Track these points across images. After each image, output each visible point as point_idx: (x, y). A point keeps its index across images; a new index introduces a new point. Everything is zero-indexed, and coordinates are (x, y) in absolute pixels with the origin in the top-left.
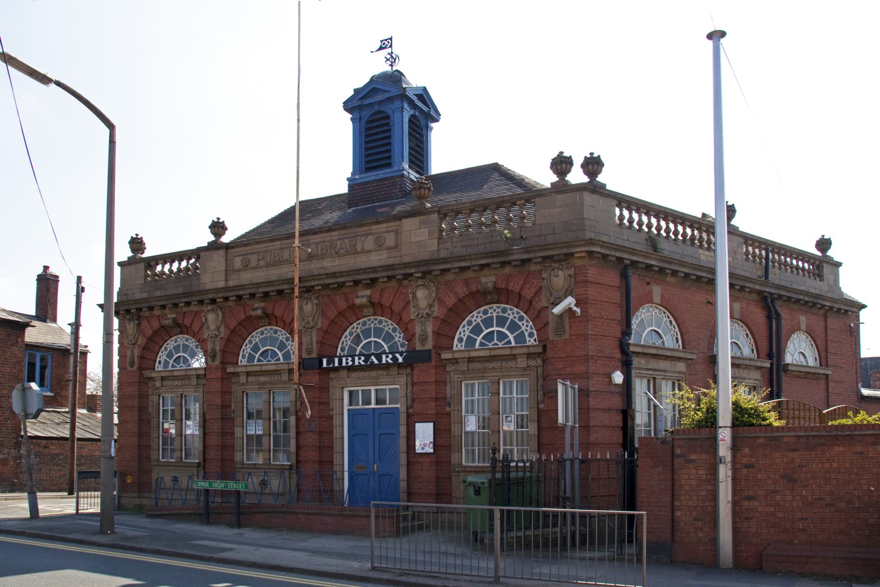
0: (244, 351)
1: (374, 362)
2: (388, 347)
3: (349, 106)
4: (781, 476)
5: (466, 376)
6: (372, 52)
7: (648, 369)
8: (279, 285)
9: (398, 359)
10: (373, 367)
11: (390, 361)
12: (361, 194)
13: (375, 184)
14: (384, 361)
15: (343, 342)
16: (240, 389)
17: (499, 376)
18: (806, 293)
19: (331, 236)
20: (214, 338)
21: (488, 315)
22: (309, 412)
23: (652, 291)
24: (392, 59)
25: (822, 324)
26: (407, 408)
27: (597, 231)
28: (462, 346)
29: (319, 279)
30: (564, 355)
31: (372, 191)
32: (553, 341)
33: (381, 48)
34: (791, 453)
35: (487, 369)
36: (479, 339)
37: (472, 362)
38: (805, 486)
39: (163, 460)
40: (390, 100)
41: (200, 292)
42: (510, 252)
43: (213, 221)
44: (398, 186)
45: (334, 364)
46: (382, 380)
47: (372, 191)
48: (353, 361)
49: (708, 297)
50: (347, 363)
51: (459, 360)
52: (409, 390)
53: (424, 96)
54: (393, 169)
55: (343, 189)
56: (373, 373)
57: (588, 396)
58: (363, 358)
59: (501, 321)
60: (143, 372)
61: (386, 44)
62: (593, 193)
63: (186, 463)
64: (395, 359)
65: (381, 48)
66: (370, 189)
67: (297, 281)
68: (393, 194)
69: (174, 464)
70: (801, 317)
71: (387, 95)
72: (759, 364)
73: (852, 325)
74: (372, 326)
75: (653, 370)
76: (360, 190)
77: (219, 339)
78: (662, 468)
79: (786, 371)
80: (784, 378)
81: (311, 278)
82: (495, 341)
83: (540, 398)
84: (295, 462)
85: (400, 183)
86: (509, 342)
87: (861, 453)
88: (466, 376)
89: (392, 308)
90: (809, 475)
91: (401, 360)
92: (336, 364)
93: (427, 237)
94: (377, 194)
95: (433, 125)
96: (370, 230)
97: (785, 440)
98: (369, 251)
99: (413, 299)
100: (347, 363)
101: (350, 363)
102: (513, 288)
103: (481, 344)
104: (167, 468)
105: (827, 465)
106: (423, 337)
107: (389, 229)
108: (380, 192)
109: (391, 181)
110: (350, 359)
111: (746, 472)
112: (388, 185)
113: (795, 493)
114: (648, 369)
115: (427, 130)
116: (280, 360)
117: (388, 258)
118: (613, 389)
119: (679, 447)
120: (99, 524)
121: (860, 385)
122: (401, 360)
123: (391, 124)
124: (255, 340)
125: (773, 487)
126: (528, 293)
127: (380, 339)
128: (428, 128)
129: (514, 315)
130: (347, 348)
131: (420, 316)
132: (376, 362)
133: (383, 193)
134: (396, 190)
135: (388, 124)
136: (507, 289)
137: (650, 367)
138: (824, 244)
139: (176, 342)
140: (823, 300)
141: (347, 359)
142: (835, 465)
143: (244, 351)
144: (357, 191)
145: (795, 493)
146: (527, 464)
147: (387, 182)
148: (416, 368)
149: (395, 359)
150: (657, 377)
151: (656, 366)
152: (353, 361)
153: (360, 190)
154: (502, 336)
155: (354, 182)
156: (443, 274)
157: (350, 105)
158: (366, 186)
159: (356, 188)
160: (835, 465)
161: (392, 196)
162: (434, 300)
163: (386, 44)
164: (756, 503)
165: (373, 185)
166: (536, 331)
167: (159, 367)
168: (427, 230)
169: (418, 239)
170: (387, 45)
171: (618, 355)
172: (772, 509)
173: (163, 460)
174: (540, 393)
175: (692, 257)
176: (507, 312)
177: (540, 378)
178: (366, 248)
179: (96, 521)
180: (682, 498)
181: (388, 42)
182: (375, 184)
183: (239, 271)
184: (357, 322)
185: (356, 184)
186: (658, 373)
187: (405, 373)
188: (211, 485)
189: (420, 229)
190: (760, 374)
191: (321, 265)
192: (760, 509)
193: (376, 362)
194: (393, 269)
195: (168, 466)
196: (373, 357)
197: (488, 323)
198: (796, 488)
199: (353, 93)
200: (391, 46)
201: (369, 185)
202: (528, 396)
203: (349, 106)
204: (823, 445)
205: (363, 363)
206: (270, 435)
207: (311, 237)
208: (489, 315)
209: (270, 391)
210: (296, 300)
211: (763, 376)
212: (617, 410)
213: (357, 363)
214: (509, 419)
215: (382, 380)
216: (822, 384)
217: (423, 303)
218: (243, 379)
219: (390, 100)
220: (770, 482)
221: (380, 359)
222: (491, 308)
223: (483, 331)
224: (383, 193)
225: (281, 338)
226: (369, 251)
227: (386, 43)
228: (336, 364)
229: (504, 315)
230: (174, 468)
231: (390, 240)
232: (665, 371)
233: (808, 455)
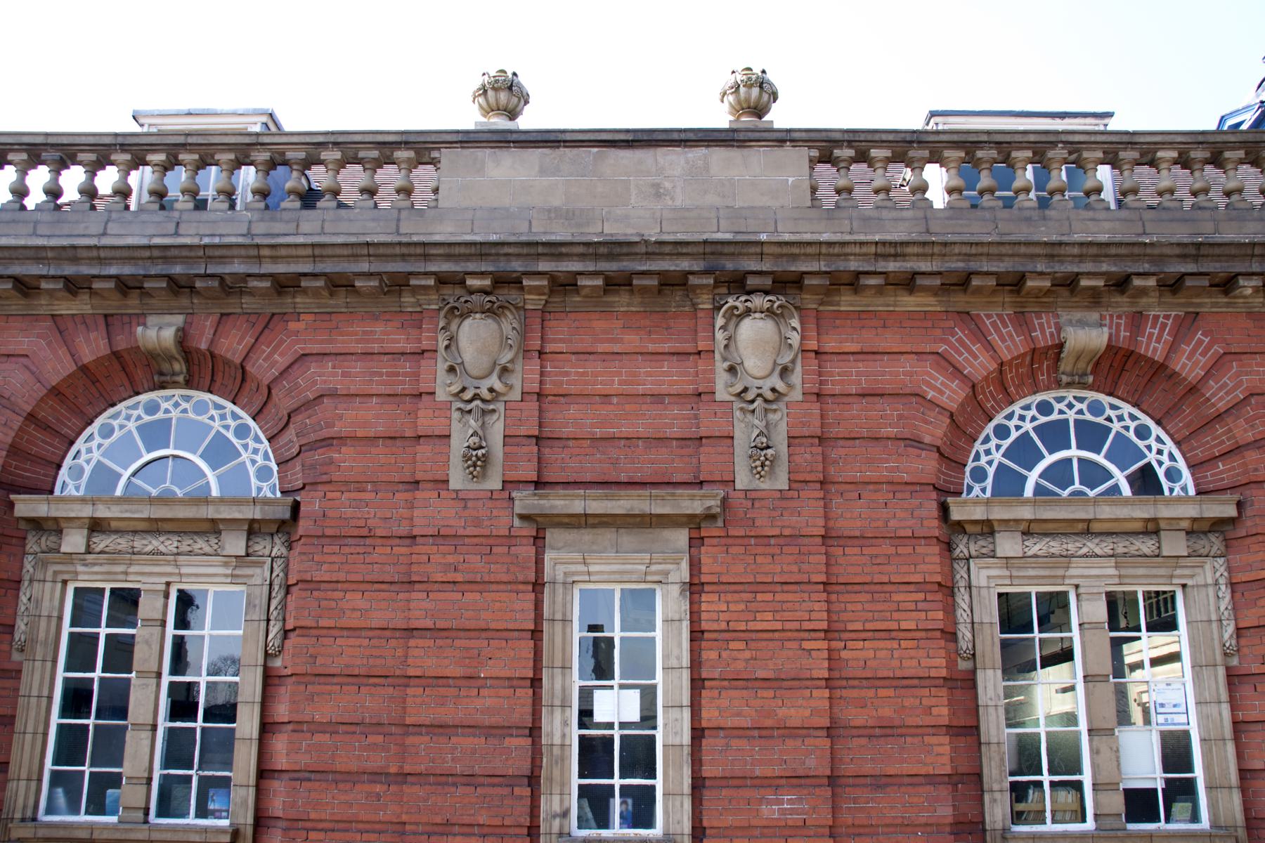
2: (220, 478)
5: (1015, 573)
16: (56, 573)
17: (170, 574)
20: (484, 401)
21: (200, 418)
26: (266, 654)
28: (984, 490)
32: (457, 491)
35: (139, 553)
36: (1033, 477)
37: (103, 531)
51: (1163, 525)
52: (274, 603)
59: (1092, 435)
60: (12, 497)
63: (160, 828)
77: (500, 407)
82: (1077, 486)
83: (1230, 642)
84: (250, 820)
86: (1116, 489)
88: (1015, 573)
89: (248, 368)
99: (447, 347)
102: (1147, 349)
103: (1039, 490)
106: (480, 452)
124: (1018, 428)
126: (264, 367)
127: (194, 453)
129: (1028, 419)
131: (468, 395)
136: (213, 356)
154: (1093, 474)
156: (280, 294)
162: (796, 356)
166: (278, 465)
167: (69, 483)
173: (584, 833)
174: (275, 629)
176: (207, 411)
177: (276, 588)
187: (267, 552)
194: (560, 257)
197: (1055, 435)
202: (241, 632)
206: (154, 727)
209: (168, 584)
217: (755, 363)
218: (74, 541)
222: (1060, 400)
223: (1098, 452)
225: (1028, 426)
229: (200, 418)
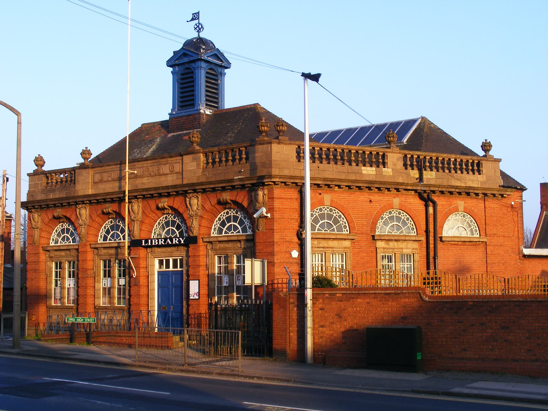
0: (101, 234)
1: (169, 243)
3: (170, 63)
4: (336, 315)
6: (187, 21)
7: (318, 247)
8: (118, 194)
9: (181, 241)
10: (168, 246)
11: (177, 243)
12: (176, 124)
13: (185, 118)
14: (174, 243)
15: (155, 229)
18: (456, 187)
19: (147, 164)
22: (135, 274)
23: (324, 199)
24: (199, 28)
25: (483, 205)
27: (281, 167)
29: (139, 192)
30: (263, 241)
31: (183, 123)
33: (193, 19)
34: (340, 302)
38: (345, 320)
39: (54, 305)
40: (194, 61)
41: (74, 197)
42: (234, 180)
43: (83, 150)
44: (197, 120)
45: (148, 244)
46: (175, 254)
47: (183, 123)
48: (158, 242)
49: (370, 197)
50: (155, 243)
53: (218, 55)
54: (194, 109)
55: (167, 118)
56: (169, 249)
57: (274, 266)
58: (163, 240)
61: (196, 16)
62: (279, 144)
64: (179, 241)
65: (193, 19)
66: (182, 121)
67: (127, 193)
68: (195, 126)
69: (60, 307)
70: (459, 202)
71: (191, 59)
72: (417, 239)
73: (513, 203)
74: (170, 219)
75: (323, 248)
76: (176, 122)
78: (283, 310)
79: (441, 241)
80: (440, 245)
81: (135, 191)
85: (198, 118)
87: (369, 303)
90: (348, 314)
91: (182, 242)
92: (150, 244)
93: (195, 168)
94: (186, 125)
95: (226, 71)
96: (168, 161)
97: (338, 295)
98: (167, 174)
100: (155, 243)
101: (157, 243)
104: (56, 310)
105: (355, 309)
107: (177, 161)
108: (187, 123)
109: (194, 117)
110: (157, 240)
111: (321, 312)
112: (192, 119)
113: (341, 324)
114: (318, 247)
115: (221, 76)
116: (121, 240)
117: (177, 179)
118: (291, 260)
119: (292, 298)
120: (12, 344)
121: (522, 247)
122: (182, 242)
123: (194, 77)
125: (332, 321)
128: (223, 74)
130: (157, 233)
132: (170, 243)
133: (189, 124)
134: (197, 123)
135: (192, 77)
137: (321, 246)
138: (486, 147)
139: (62, 227)
140: (474, 189)
141: (155, 241)
142: (358, 309)
143: (101, 234)
144: (175, 122)
145: (341, 324)
146: (247, 306)
147: (191, 117)
148: (190, 247)
149: (179, 241)
150: (326, 252)
151: (326, 245)
152: (158, 242)
153: (176, 122)
154: (236, 228)
155: (173, 116)
157: (173, 63)
158: (179, 119)
159: (174, 120)
160: (358, 309)
161: (194, 127)
163: (196, 16)
164: (325, 329)
165: (183, 118)
168: (195, 163)
169: (191, 169)
170: (196, 17)
171: (296, 240)
172: (332, 332)
175: (356, 173)
178: (165, 172)
179: (11, 343)
180: (293, 326)
181: (197, 15)
182: (185, 118)
183: (97, 183)
184: (162, 217)
185: (174, 117)
186: (327, 249)
188: (76, 320)
189: (192, 162)
190: (418, 244)
191: (141, 182)
192: (327, 332)
193: (170, 243)
195: (57, 308)
196: (168, 240)
198: (342, 321)
199: (173, 55)
200: (198, 18)
201: (181, 119)
203: (170, 63)
204: (353, 298)
205: (163, 243)
207: (136, 163)
208: (229, 215)
210: (127, 205)
211: (421, 245)
212: (296, 273)
213: (160, 244)
214: (239, 278)
215: (175, 254)
216: (481, 249)
219: (194, 61)
220: (331, 318)
221: (172, 241)
224: (189, 124)
226: (167, 174)
227: (196, 16)
228: (150, 244)
230: (60, 310)
231: (178, 168)
232: (333, 248)
233: (347, 303)
